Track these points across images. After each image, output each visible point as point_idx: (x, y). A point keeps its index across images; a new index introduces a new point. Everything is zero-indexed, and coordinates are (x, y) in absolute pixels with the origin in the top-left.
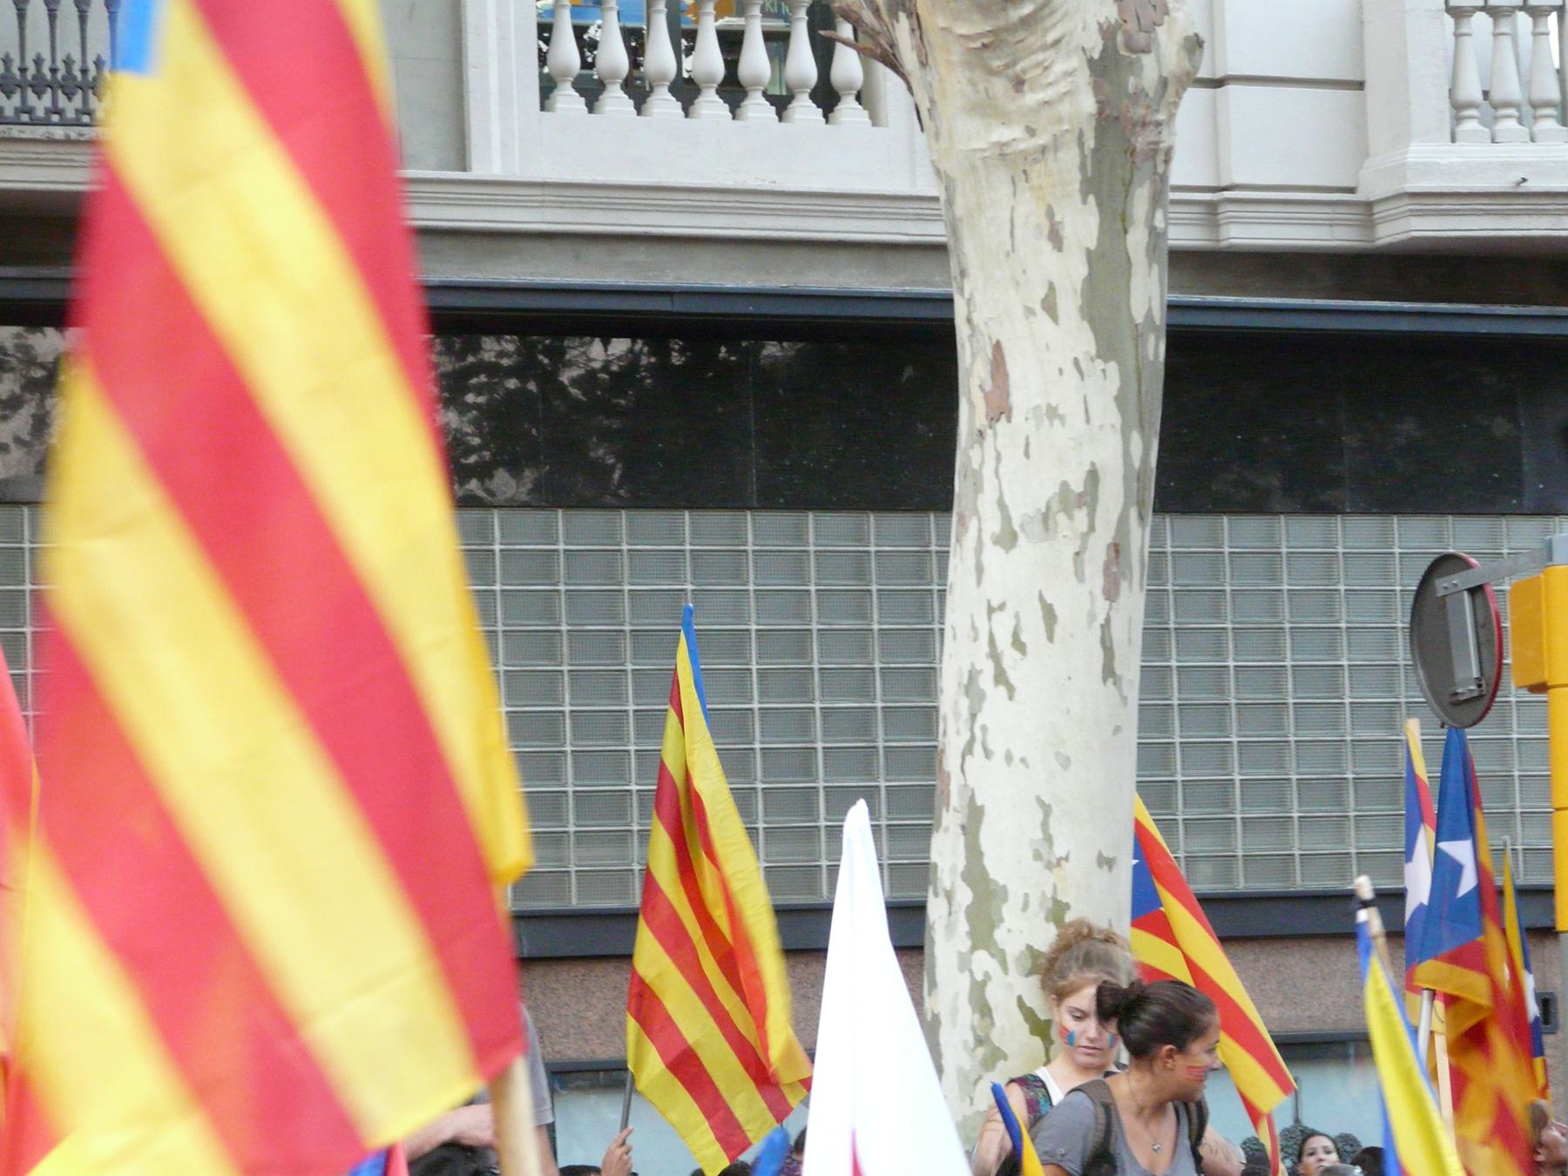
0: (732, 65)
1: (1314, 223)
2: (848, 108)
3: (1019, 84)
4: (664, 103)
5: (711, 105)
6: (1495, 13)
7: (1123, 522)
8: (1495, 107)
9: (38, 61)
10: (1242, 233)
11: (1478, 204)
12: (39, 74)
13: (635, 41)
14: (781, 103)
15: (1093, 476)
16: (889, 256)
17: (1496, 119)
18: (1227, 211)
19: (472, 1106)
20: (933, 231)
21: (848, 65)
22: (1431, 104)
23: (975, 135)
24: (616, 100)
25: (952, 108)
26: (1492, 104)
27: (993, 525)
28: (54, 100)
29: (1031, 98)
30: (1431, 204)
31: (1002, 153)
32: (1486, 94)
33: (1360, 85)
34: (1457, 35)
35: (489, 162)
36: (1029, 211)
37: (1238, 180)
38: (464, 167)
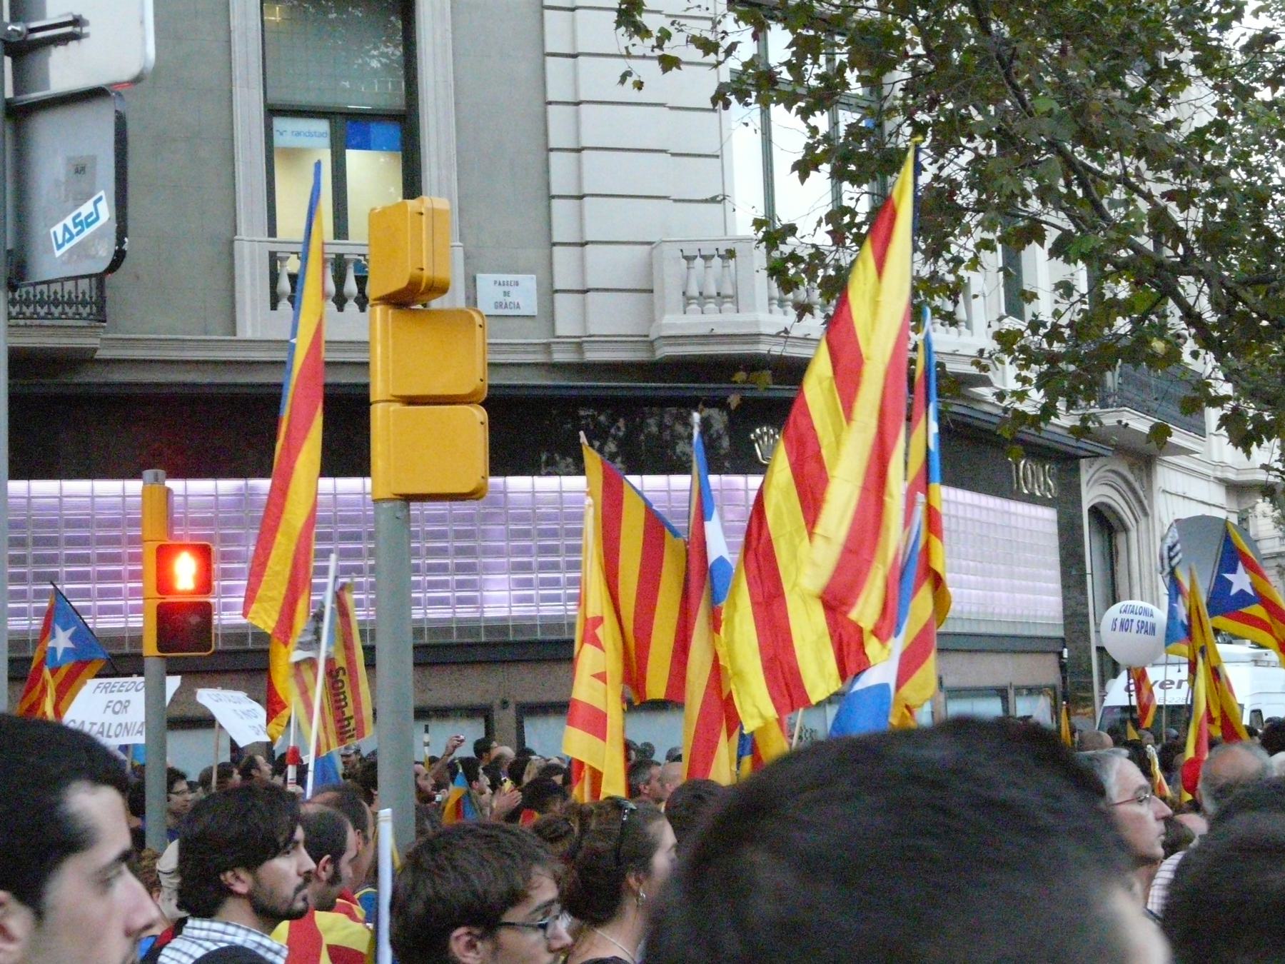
0: (362, 290)
1: (623, 350)
6: (706, 258)
8: (705, 298)
9: (84, 293)
10: (592, 356)
11: (695, 340)
12: (56, 299)
16: (201, 366)
17: (723, 303)
18: (586, 346)
19: (1058, 670)
20: (280, 356)
22: (675, 297)
26: (703, 297)
28: (35, 309)
30: (672, 341)
32: (701, 294)
33: (651, 291)
34: (688, 268)
35: (247, 330)
37: (592, 332)
38: (235, 335)
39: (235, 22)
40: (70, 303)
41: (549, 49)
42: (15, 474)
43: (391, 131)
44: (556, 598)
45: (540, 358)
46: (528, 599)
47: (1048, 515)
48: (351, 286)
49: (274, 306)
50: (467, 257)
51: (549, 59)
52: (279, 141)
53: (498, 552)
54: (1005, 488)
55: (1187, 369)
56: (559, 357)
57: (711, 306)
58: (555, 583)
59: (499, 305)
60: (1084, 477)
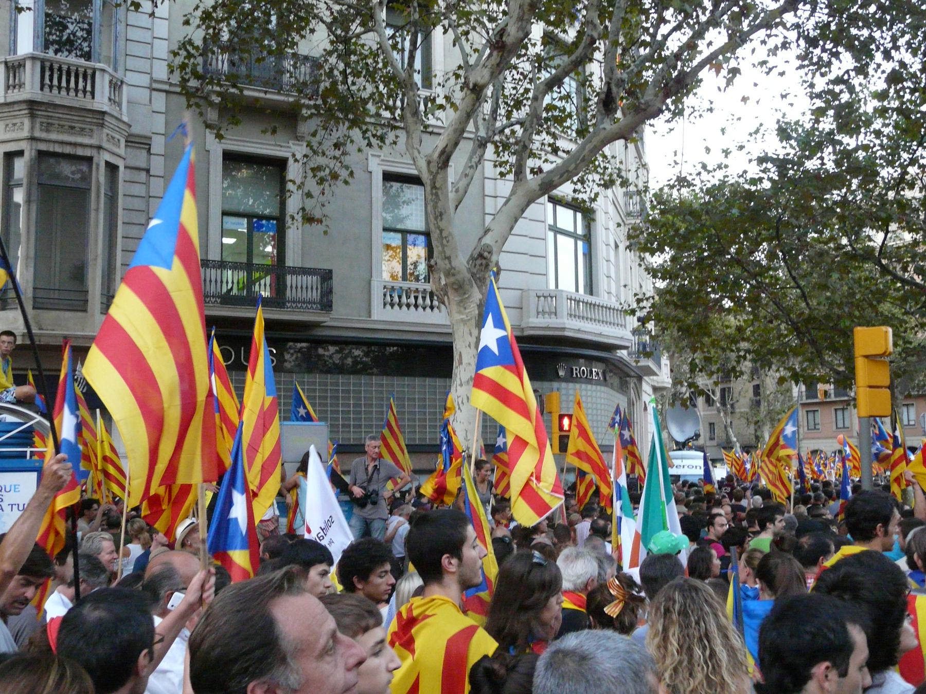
2: (436, 310)
4: (404, 308)
5: (412, 308)
6: (545, 297)
10: (526, 333)
13: (400, 297)
14: (424, 308)
20: (450, 331)
21: (436, 303)
22: (533, 312)
23: (458, 317)
24: (396, 307)
25: (454, 312)
26: (544, 312)
27: (459, 382)
29: (467, 311)
31: (462, 320)
35: (375, 317)
36: (466, 330)
39: (373, 195)
40: (309, 303)
41: (166, 22)
51: (166, 37)
55: (245, 369)
57: (546, 316)
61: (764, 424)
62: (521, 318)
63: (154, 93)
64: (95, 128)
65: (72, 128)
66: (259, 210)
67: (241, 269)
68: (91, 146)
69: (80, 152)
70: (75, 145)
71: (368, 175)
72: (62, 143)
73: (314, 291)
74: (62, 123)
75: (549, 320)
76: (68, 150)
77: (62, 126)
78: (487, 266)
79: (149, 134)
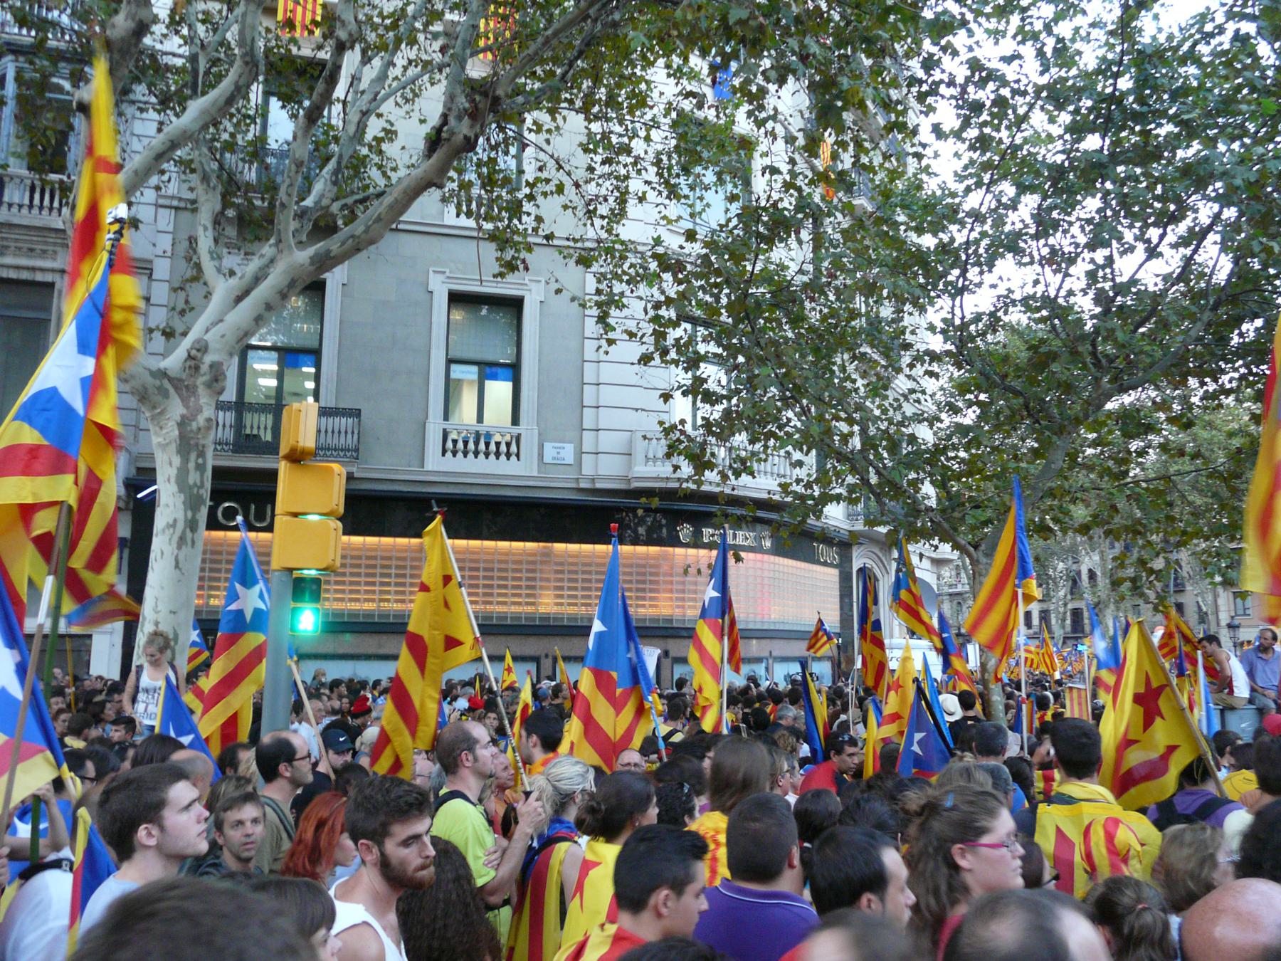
2: (513, 458)
3: (161, 428)
7: (184, 532)
10: (599, 485)
15: (175, 521)
29: (164, 431)
35: (429, 466)
36: (166, 458)
39: (434, 319)
42: (344, 534)
43: (509, 372)
44: (575, 605)
45: (574, 485)
46: (561, 604)
47: (835, 572)
48: (482, 446)
49: (443, 455)
50: (540, 434)
52: (453, 375)
53: (548, 580)
54: (812, 558)
56: (583, 485)
57: (659, 463)
58: (575, 597)
59: (554, 458)
60: (855, 554)
61: (1106, 606)
62: (630, 467)
63: (161, 211)
64: (58, 249)
65: (32, 250)
66: (490, 356)
67: (229, 409)
68: (53, 270)
69: (39, 277)
70: (33, 269)
71: (428, 296)
72: (17, 268)
73: (349, 436)
74: (19, 245)
75: (662, 469)
76: (25, 275)
77: (20, 249)
78: (197, 368)
79: (152, 257)
